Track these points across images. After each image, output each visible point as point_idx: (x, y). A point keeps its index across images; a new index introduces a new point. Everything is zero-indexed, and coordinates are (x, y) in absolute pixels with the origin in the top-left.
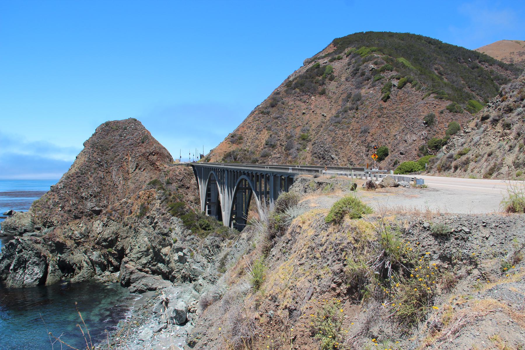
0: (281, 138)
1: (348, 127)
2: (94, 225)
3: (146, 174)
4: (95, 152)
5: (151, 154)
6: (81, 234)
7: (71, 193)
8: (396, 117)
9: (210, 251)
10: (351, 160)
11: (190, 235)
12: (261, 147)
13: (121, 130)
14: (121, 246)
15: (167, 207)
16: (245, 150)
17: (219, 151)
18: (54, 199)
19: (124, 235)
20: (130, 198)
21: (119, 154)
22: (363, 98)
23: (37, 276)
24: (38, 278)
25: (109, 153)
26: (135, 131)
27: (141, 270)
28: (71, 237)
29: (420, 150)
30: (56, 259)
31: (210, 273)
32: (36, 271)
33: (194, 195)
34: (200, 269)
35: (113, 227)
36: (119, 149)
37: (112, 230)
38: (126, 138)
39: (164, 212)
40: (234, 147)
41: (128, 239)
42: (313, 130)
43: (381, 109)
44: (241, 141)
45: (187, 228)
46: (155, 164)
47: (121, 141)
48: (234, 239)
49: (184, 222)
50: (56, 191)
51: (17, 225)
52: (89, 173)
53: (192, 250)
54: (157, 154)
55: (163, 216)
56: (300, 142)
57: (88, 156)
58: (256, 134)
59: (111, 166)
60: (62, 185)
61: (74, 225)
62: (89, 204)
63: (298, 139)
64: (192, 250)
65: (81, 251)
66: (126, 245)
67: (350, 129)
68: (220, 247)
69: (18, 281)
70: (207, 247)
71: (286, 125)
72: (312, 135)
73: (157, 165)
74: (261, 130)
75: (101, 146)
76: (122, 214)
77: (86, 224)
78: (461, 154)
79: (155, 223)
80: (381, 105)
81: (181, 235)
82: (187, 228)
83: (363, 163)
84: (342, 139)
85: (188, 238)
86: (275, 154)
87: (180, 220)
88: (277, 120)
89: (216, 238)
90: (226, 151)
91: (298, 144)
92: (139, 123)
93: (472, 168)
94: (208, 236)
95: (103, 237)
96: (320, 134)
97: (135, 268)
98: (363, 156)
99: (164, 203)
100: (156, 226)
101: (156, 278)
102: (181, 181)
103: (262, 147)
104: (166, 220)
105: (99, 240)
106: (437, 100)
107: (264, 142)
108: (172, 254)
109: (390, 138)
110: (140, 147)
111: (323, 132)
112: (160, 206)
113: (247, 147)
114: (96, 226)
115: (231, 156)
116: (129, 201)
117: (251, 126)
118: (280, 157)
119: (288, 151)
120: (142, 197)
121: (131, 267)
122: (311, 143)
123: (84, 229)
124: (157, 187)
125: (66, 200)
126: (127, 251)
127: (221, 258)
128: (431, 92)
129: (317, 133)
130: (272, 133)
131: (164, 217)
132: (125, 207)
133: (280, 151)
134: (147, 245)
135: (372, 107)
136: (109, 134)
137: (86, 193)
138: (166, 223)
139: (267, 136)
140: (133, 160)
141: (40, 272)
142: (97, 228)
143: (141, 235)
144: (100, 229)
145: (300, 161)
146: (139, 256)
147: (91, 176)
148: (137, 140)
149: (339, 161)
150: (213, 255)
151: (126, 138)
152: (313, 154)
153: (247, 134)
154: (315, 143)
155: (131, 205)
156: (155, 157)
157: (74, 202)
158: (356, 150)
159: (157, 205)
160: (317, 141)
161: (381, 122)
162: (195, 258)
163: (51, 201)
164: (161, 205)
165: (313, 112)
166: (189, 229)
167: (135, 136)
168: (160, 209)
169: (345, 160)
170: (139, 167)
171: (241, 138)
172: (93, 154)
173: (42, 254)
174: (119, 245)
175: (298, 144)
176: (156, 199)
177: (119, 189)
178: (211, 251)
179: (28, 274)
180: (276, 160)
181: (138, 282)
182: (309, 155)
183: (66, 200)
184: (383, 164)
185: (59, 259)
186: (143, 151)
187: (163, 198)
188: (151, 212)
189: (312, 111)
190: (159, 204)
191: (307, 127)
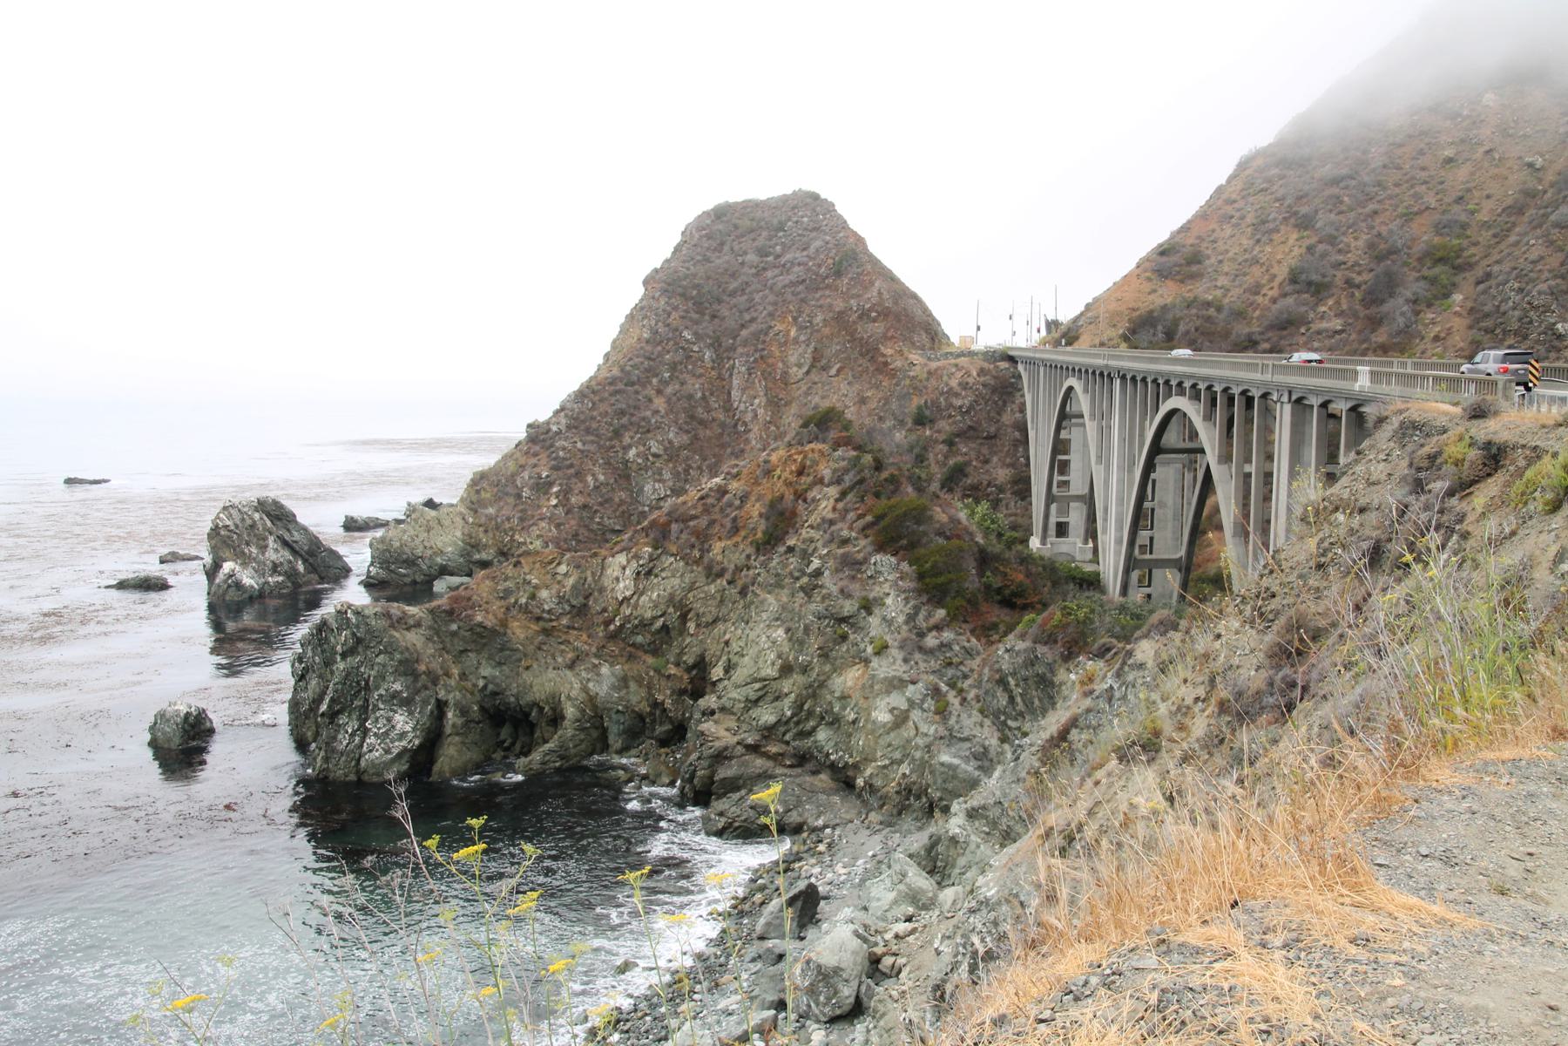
0: (1351, 258)
2: (609, 571)
3: (844, 388)
4: (676, 308)
5: (864, 315)
6: (561, 599)
7: (592, 448)
9: (1012, 699)
11: (938, 628)
13: (765, 234)
15: (860, 517)
16: (1208, 304)
17: (1113, 306)
18: (535, 466)
19: (709, 611)
20: (736, 476)
21: (755, 315)
23: (404, 743)
24: (405, 750)
25: (725, 312)
26: (814, 234)
27: (754, 749)
28: (525, 610)
30: (475, 685)
31: (998, 793)
32: (399, 726)
33: (1012, 465)
34: (969, 768)
35: (672, 579)
36: (757, 297)
37: (669, 590)
38: (783, 260)
39: (845, 533)
40: (1168, 294)
41: (721, 627)
42: (1485, 225)
44: (1194, 268)
45: (929, 601)
46: (877, 349)
47: (764, 269)
48: (1108, 656)
49: (921, 576)
50: (544, 440)
51: (419, 552)
52: (655, 381)
53: (944, 688)
54: (886, 315)
55: (841, 551)
56: (1425, 272)
57: (653, 323)
58: (1251, 242)
59: (729, 359)
60: (564, 421)
61: (538, 565)
62: (648, 488)
63: (1420, 260)
64: (944, 688)
65: (560, 660)
66: (713, 648)
68: (1052, 684)
69: (342, 754)
70: (1002, 682)
71: (1371, 207)
72: (1476, 244)
74: (1271, 226)
75: (696, 286)
76: (703, 537)
77: (578, 567)
79: (810, 575)
81: (904, 627)
82: (929, 601)
85: (931, 641)
86: (1322, 318)
87: (905, 566)
89: (1038, 646)
90: (1135, 305)
91: (1417, 280)
92: (829, 208)
94: (1011, 636)
96: (1513, 238)
97: (736, 739)
99: (849, 497)
100: (816, 587)
101: (807, 786)
103: (1274, 293)
104: (853, 566)
105: (622, 626)
107: (1282, 272)
108: (867, 698)
110: (827, 292)
111: (1526, 234)
112: (834, 509)
114: (616, 574)
115: (1154, 326)
116: (734, 485)
117: (1237, 215)
118: (1342, 331)
119: (1373, 310)
120: (778, 472)
121: (723, 733)
122: (1471, 276)
123: (571, 581)
124: (833, 434)
125: (572, 471)
126: (717, 672)
127: (1045, 735)
129: (1500, 237)
130: (1313, 240)
131: (843, 555)
132: (717, 509)
133: (1344, 307)
136: (726, 248)
137: (641, 448)
138: (853, 578)
139: (1296, 251)
140: (802, 338)
141: (414, 729)
142: (617, 579)
143: (764, 616)
144: (624, 587)
145: (1422, 347)
146: (753, 696)
147: (659, 392)
148: (820, 266)
150: (1021, 714)
151: (783, 260)
153: (1220, 243)
154: (1488, 276)
155: (737, 502)
156: (878, 328)
157: (602, 478)
159: (825, 508)
160: (1496, 268)
162: (952, 721)
163: (526, 475)
164: (840, 505)
165: (1488, 152)
166: (940, 603)
167: (812, 249)
168: (832, 522)
170: (824, 362)
171: (1195, 259)
172: (669, 315)
173: (423, 668)
174: (692, 644)
175: (1417, 280)
176: (826, 481)
177: (751, 435)
178: (1019, 699)
179: (375, 734)
181: (736, 796)
183: (572, 471)
185: (485, 687)
186: (839, 305)
187: (848, 479)
188: (804, 531)
189: (1482, 150)
190: (832, 501)
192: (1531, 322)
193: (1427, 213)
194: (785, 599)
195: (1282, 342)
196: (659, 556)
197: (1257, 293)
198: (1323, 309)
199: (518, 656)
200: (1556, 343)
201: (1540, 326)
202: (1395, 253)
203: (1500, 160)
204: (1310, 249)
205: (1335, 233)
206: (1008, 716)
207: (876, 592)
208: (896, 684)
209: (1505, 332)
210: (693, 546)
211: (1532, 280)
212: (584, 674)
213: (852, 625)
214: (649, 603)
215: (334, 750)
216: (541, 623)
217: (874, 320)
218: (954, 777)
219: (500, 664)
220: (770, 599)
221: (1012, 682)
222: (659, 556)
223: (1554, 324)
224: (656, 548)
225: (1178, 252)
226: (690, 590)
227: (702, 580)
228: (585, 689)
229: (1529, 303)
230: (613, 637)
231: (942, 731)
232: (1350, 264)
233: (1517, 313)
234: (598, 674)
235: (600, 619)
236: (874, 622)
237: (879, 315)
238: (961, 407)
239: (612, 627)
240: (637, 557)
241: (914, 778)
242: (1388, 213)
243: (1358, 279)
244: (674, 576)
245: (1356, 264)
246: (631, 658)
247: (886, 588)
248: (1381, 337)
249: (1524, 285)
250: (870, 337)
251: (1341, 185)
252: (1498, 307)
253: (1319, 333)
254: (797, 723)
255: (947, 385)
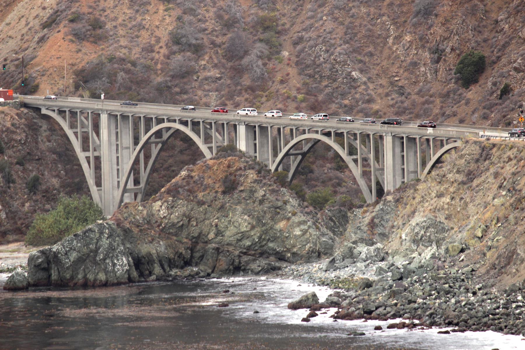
6: (144, 219)
9: (335, 223)
63: (253, 27)
70: (331, 219)
83: (429, 91)
86: (204, 69)
93: (324, 273)
95: (170, 221)
98: (426, 73)
102: (25, 144)
105: (165, 227)
109: (485, 26)
113: (124, 51)
123: (145, 212)
133: (216, 61)
134: (249, 224)
146: (239, 238)
149: (371, 86)
152: (303, 70)
158: (409, 60)
169: (383, 81)
178: (337, 223)
182: (293, 71)
192: (337, 71)
194: (244, 207)
195: (186, 87)
196: (176, 200)
197: (153, 51)
198: (203, 63)
199: (136, 239)
200: (353, 84)
201: (342, 74)
204: (179, 19)
205: (193, 7)
206: (335, 228)
208: (300, 223)
209: (321, 77)
210: (189, 196)
211: (333, 45)
212: (156, 245)
213: (280, 209)
214: (175, 218)
215: (108, 271)
216: (140, 228)
218: (328, 244)
219: (131, 243)
220: (238, 207)
221: (334, 218)
222: (176, 200)
223: (350, 72)
226: (192, 210)
227: (196, 207)
230: (162, 230)
231: (320, 233)
232: (210, 30)
233: (328, 66)
234: (160, 244)
235: (155, 225)
236: (289, 208)
238: (20, 140)
239: (161, 227)
240: (167, 201)
241: (314, 247)
243: (219, 41)
244: (183, 207)
245: (214, 30)
246: (168, 238)
248: (246, 81)
249: (328, 48)
252: (314, 61)
253: (206, 79)
254: (260, 243)
255: (4, 126)
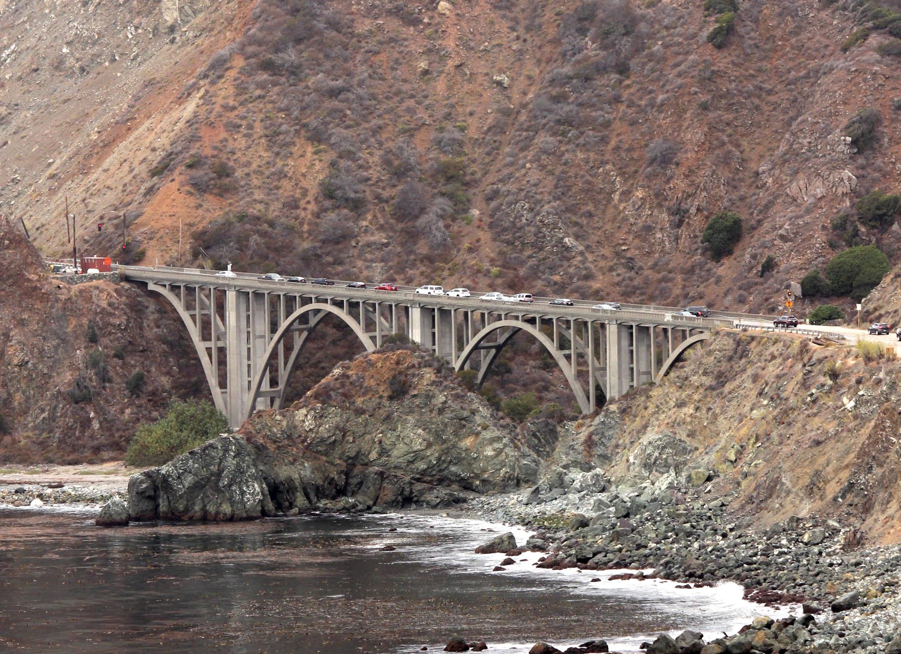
1: (604, 140)
6: (283, 432)
8: (757, 108)
10: (629, 255)
12: (310, 207)
14: (356, 449)
22: (643, 27)
29: (835, 228)
35: (334, 417)
42: (476, 142)
43: (709, 78)
49: (488, 400)
63: (432, 176)
67: (610, 147)
72: (474, 161)
73: (29, 280)
78: (876, 309)
80: (708, 64)
84: (589, 183)
86: (366, 231)
88: (335, 103)
93: (524, 507)
98: (663, 241)
103: (312, 207)
106: (888, 60)
109: (741, 180)
113: (259, 207)
123: (284, 423)
128: (870, 24)
133: (382, 221)
135: (677, 65)
142: (304, 421)
143: (409, 425)
146: (411, 459)
149: (590, 257)
152: (498, 234)
153: (239, 154)
158: (640, 223)
161: (712, 128)
169: (607, 251)
180: (378, 254)
182: (485, 236)
184: (726, 269)
191: (451, 132)
192: (544, 237)
193: (423, 130)
195: (341, 255)
198: (365, 223)
200: (565, 254)
202: (410, 170)
203: (471, 74)
204: (333, 164)
205: (352, 149)
207: (474, 407)
208: (493, 440)
213: (467, 421)
214: (324, 430)
215: (234, 502)
217: (8, 247)
220: (409, 418)
223: (562, 239)
224: (323, 404)
225: (205, 164)
226: (347, 422)
227: (353, 417)
228: (300, 474)
229: (541, 221)
230: (307, 448)
232: (374, 180)
233: (533, 229)
236: (478, 419)
237: (11, 243)
240: (314, 409)
242: (390, 128)
243: (385, 194)
247: (477, 405)
249: (533, 206)
250: (10, 263)
251: (342, 96)
252: (513, 222)
253: (369, 245)
